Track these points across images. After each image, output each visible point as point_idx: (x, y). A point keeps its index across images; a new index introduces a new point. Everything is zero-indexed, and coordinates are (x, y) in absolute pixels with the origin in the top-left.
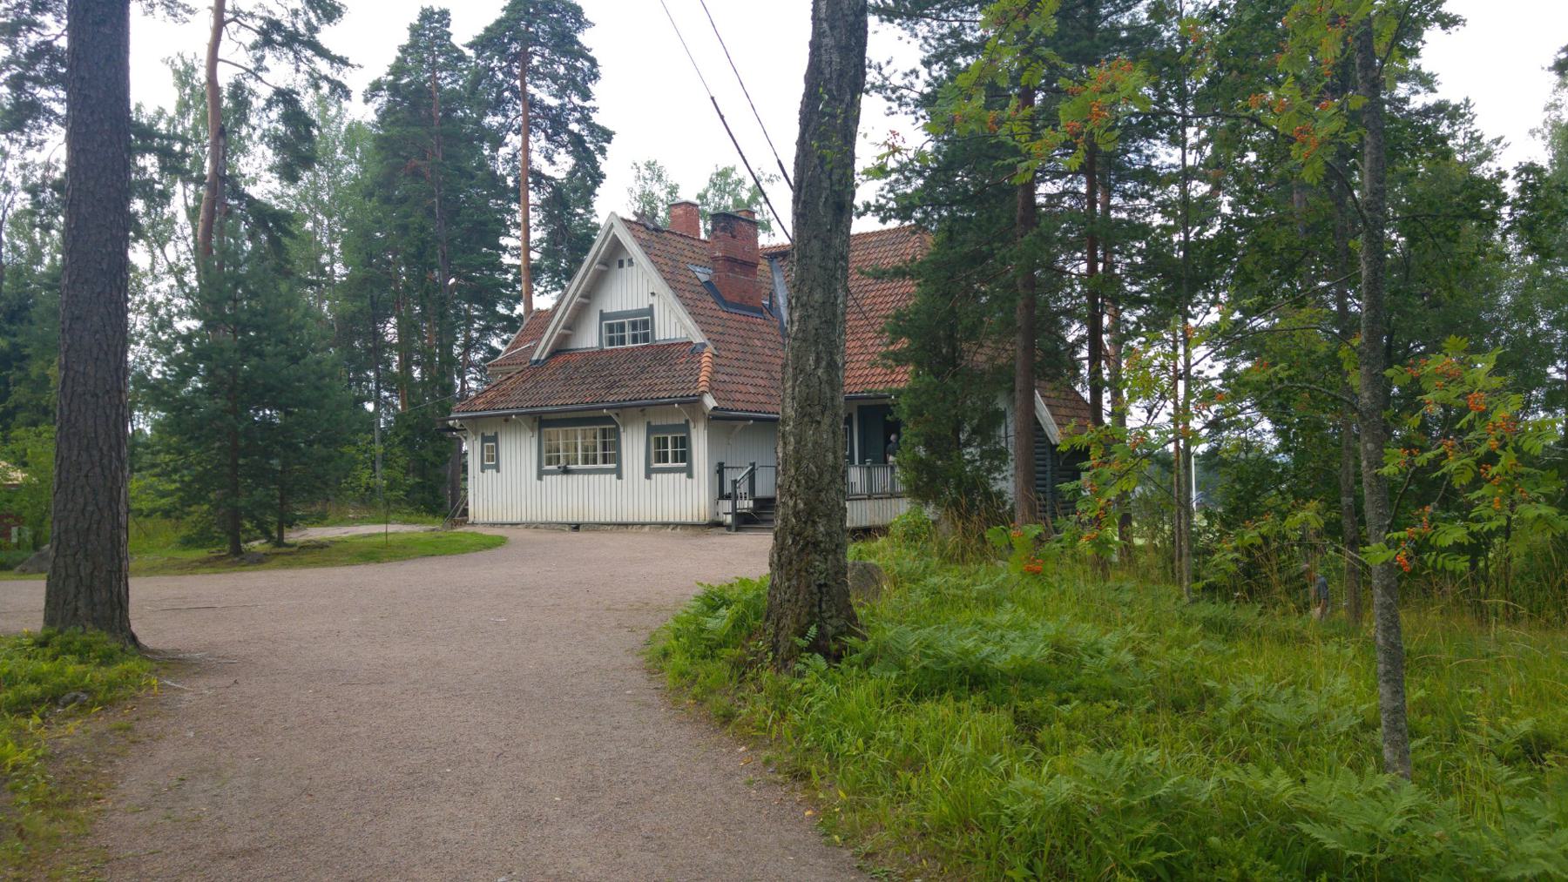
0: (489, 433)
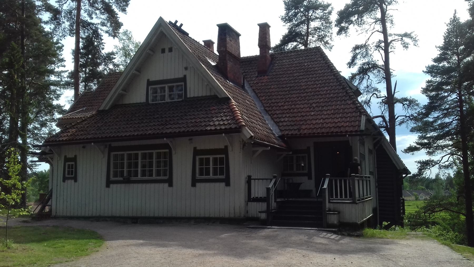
0: (70, 155)
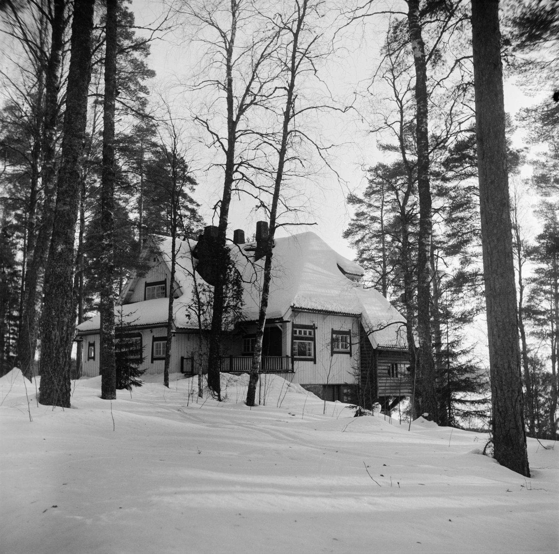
0: (92, 342)
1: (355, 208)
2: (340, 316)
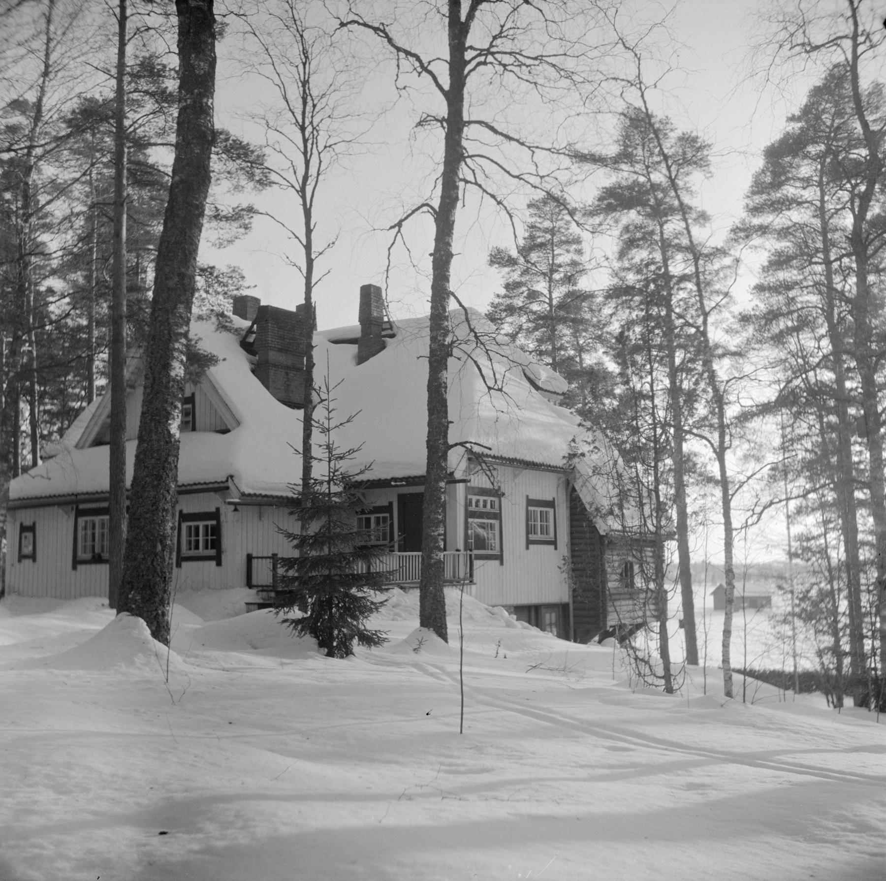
0: (28, 523)
1: (501, 275)
2: (543, 470)
